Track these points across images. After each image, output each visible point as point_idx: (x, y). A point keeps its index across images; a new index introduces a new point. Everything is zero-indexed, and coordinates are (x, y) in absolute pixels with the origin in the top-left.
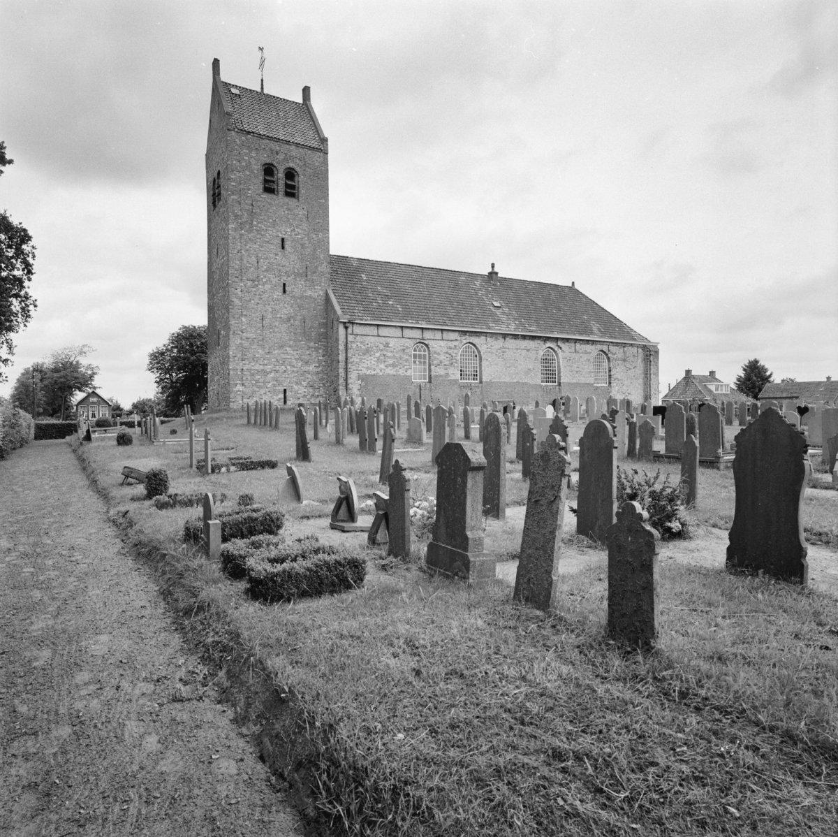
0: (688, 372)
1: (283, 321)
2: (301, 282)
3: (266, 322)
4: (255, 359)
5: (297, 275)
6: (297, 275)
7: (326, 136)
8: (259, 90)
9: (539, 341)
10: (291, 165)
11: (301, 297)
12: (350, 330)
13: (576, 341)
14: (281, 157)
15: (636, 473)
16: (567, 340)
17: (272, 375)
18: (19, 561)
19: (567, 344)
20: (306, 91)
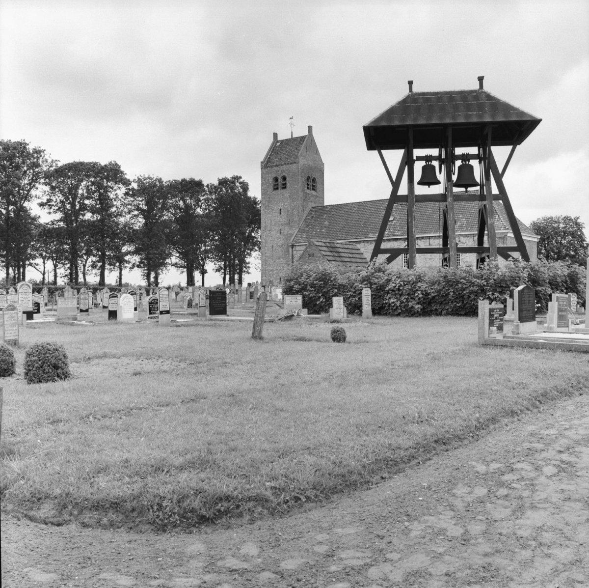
0: (516, 129)
1: (280, 247)
2: (287, 228)
3: (274, 248)
4: (269, 265)
5: (286, 224)
6: (286, 224)
7: (461, 154)
8: (383, 152)
9: (401, 241)
10: (284, 174)
11: (287, 234)
12: (294, 249)
13: (429, 238)
14: (280, 172)
15: (298, 580)
16: (422, 238)
17: (275, 272)
18: (510, 286)
19: (423, 240)
20: (310, 128)
